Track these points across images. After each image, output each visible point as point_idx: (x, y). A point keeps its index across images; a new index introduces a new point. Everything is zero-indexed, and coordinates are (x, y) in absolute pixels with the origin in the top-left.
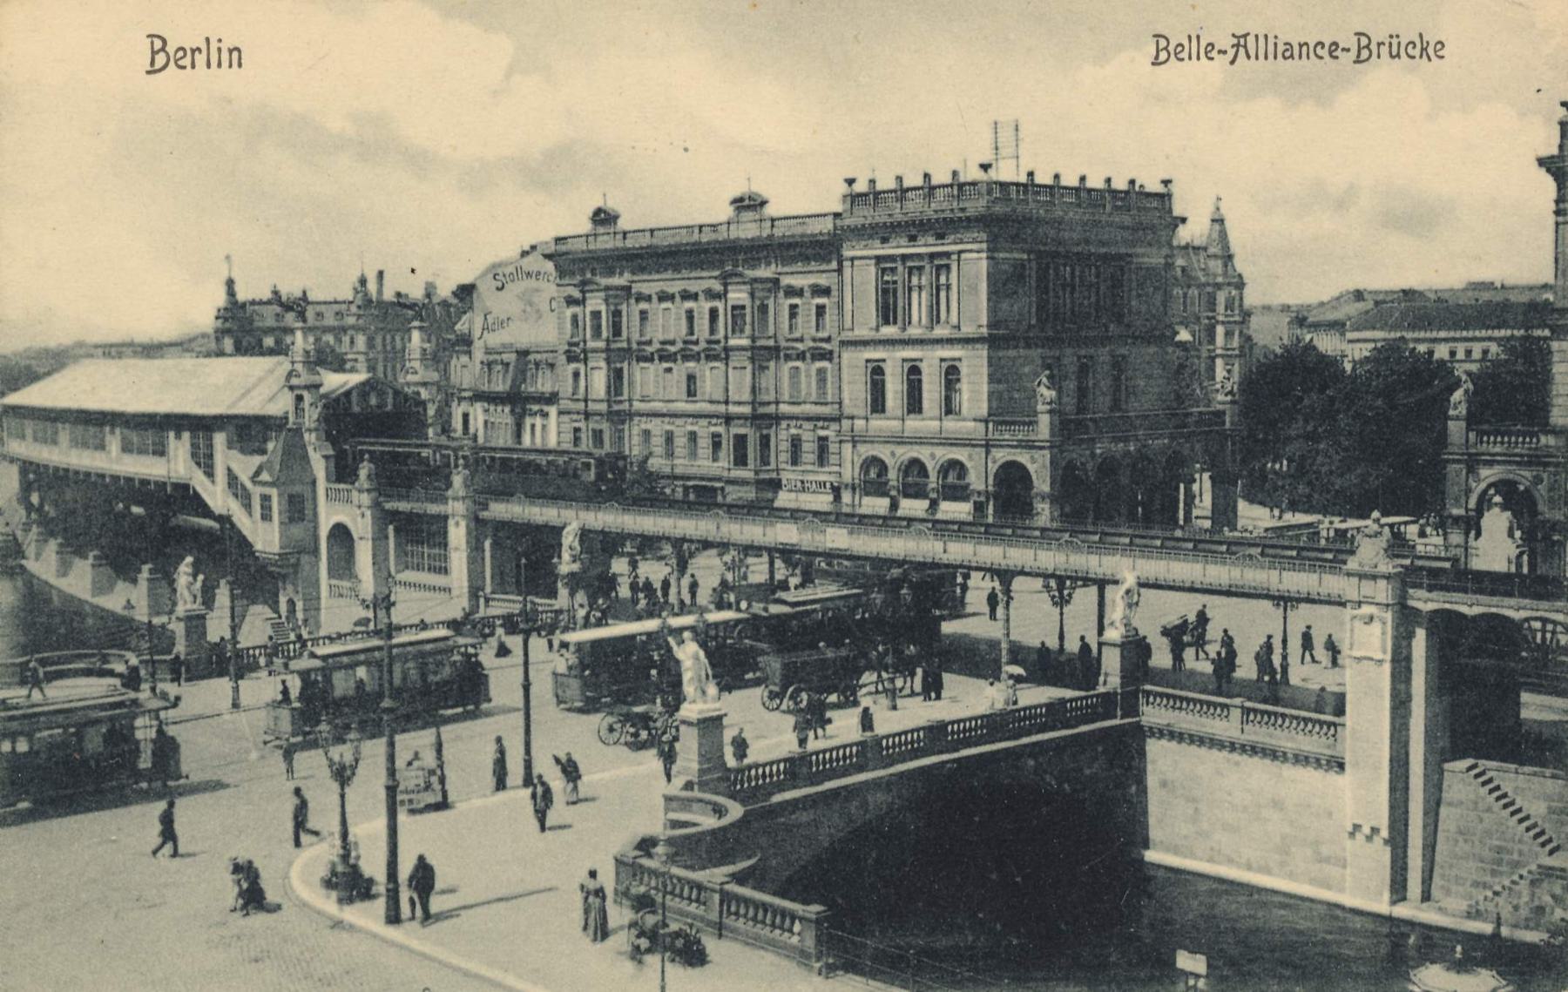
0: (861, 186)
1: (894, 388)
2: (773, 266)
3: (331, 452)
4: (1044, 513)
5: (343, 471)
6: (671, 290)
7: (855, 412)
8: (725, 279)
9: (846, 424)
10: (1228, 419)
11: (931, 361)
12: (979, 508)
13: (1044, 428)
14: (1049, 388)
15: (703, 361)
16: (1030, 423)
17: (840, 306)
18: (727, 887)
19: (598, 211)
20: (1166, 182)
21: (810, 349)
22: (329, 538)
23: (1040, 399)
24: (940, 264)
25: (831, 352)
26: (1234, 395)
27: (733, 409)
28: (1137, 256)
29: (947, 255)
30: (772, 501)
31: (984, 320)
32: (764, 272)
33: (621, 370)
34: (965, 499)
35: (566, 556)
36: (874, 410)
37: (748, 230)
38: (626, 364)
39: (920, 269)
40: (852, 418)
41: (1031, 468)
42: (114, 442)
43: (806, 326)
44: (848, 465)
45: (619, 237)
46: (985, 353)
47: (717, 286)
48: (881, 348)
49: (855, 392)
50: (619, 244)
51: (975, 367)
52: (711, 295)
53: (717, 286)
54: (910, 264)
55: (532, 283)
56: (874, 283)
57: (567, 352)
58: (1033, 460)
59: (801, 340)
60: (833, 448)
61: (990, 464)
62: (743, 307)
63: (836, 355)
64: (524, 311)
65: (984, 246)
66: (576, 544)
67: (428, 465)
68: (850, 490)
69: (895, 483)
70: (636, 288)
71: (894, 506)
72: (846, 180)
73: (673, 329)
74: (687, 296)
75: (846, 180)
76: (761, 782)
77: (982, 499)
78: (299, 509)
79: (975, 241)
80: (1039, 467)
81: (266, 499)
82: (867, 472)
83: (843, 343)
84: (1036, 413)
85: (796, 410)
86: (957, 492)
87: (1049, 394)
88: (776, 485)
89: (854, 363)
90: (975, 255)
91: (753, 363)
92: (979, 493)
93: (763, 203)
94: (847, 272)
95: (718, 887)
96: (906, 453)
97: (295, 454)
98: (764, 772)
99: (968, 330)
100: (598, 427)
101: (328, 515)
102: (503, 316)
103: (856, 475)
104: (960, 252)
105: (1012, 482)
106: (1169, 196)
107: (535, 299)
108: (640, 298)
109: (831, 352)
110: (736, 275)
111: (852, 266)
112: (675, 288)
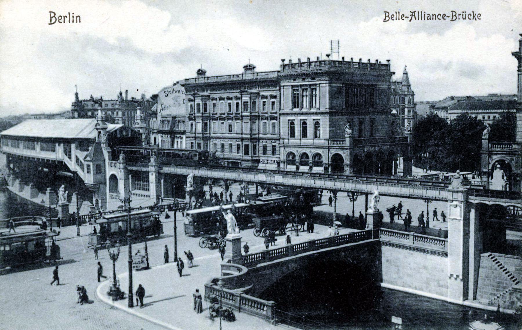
0: (287, 62)
1: (298, 129)
2: (257, 88)
4: (348, 171)
7: (285, 137)
8: (241, 93)
9: (282, 141)
10: (409, 140)
11: (310, 120)
12: (326, 169)
13: (348, 142)
14: (349, 129)
17: (280, 102)
19: (199, 70)
20: (388, 61)
21: (270, 116)
22: (109, 179)
24: (313, 88)
25: (277, 117)
26: (411, 131)
27: (244, 136)
29: (315, 85)
30: (257, 167)
32: (254, 91)
33: (207, 123)
34: (321, 166)
36: (291, 137)
37: (249, 76)
38: (208, 121)
39: (306, 89)
40: (284, 139)
41: (343, 156)
43: (268, 108)
44: (282, 155)
45: (206, 79)
46: (328, 117)
47: (239, 95)
48: (293, 116)
49: (285, 131)
50: (206, 81)
51: (325, 122)
52: (237, 98)
53: (239, 95)
54: (303, 88)
57: (189, 117)
58: (344, 153)
59: (267, 113)
60: (277, 149)
61: (329, 154)
62: (247, 102)
63: (278, 118)
65: (328, 82)
68: (283, 163)
70: (212, 96)
71: (298, 168)
74: (229, 98)
77: (327, 166)
78: (99, 169)
79: (324, 80)
80: (346, 155)
81: (88, 166)
82: (289, 157)
83: (281, 114)
84: (345, 137)
86: (319, 164)
87: (349, 131)
88: (258, 161)
89: (284, 121)
90: (324, 85)
91: (251, 121)
92: (326, 164)
94: (282, 90)
96: (302, 151)
99: (322, 110)
100: (199, 142)
101: (109, 172)
103: (285, 158)
104: (320, 84)
105: (337, 160)
106: (389, 65)
108: (213, 99)
109: (277, 117)
110: (245, 91)
111: (284, 88)
112: (225, 96)
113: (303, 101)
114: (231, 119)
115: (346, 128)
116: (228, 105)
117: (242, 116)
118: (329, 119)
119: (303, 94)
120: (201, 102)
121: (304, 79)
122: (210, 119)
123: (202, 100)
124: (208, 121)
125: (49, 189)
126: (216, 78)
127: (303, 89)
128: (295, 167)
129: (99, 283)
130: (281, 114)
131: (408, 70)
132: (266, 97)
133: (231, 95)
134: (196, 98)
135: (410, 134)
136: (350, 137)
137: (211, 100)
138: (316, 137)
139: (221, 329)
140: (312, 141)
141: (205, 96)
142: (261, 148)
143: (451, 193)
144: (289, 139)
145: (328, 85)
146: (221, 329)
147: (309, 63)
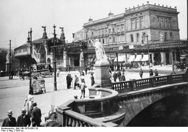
0: (128, 9)
2: (115, 22)
3: (48, 48)
5: (49, 51)
6: (100, 29)
7: (128, 42)
14: (162, 34)
15: (105, 38)
17: (125, 27)
18: (67, 112)
19: (90, 19)
20: (176, 7)
22: (47, 60)
23: (161, 36)
27: (110, 44)
28: (172, 18)
29: (143, 16)
32: (114, 23)
35: (81, 58)
40: (128, 43)
42: (22, 50)
45: (93, 22)
46: (150, 30)
47: (107, 27)
48: (132, 32)
50: (93, 23)
52: (106, 28)
53: (107, 27)
55: (82, 33)
56: (131, 24)
57: (86, 39)
63: (125, 34)
66: (83, 56)
76: (119, 89)
78: (43, 56)
79: (147, 13)
81: (38, 55)
83: (126, 32)
85: (119, 43)
89: (128, 35)
90: (147, 16)
94: (126, 22)
95: (62, 112)
97: (43, 49)
98: (118, 86)
99: (147, 27)
101: (47, 57)
102: (78, 38)
104: (144, 16)
106: (176, 9)
107: (83, 35)
108: (118, 26)
110: (109, 24)
111: (127, 21)
112: (100, 28)
113: (141, 25)
115: (160, 34)
116: (86, 34)
118: (151, 31)
119: (141, 20)
120: (111, 28)
121: (132, 16)
122: (116, 36)
123: (112, 27)
125: (79, 107)
126: (97, 21)
127: (141, 18)
129: (57, 108)
130: (126, 32)
132: (103, 29)
134: (109, 26)
137: (116, 26)
138: (138, 41)
140: (136, 43)
141: (113, 25)
143: (10, 44)
144: (136, 42)
147: (134, 8)
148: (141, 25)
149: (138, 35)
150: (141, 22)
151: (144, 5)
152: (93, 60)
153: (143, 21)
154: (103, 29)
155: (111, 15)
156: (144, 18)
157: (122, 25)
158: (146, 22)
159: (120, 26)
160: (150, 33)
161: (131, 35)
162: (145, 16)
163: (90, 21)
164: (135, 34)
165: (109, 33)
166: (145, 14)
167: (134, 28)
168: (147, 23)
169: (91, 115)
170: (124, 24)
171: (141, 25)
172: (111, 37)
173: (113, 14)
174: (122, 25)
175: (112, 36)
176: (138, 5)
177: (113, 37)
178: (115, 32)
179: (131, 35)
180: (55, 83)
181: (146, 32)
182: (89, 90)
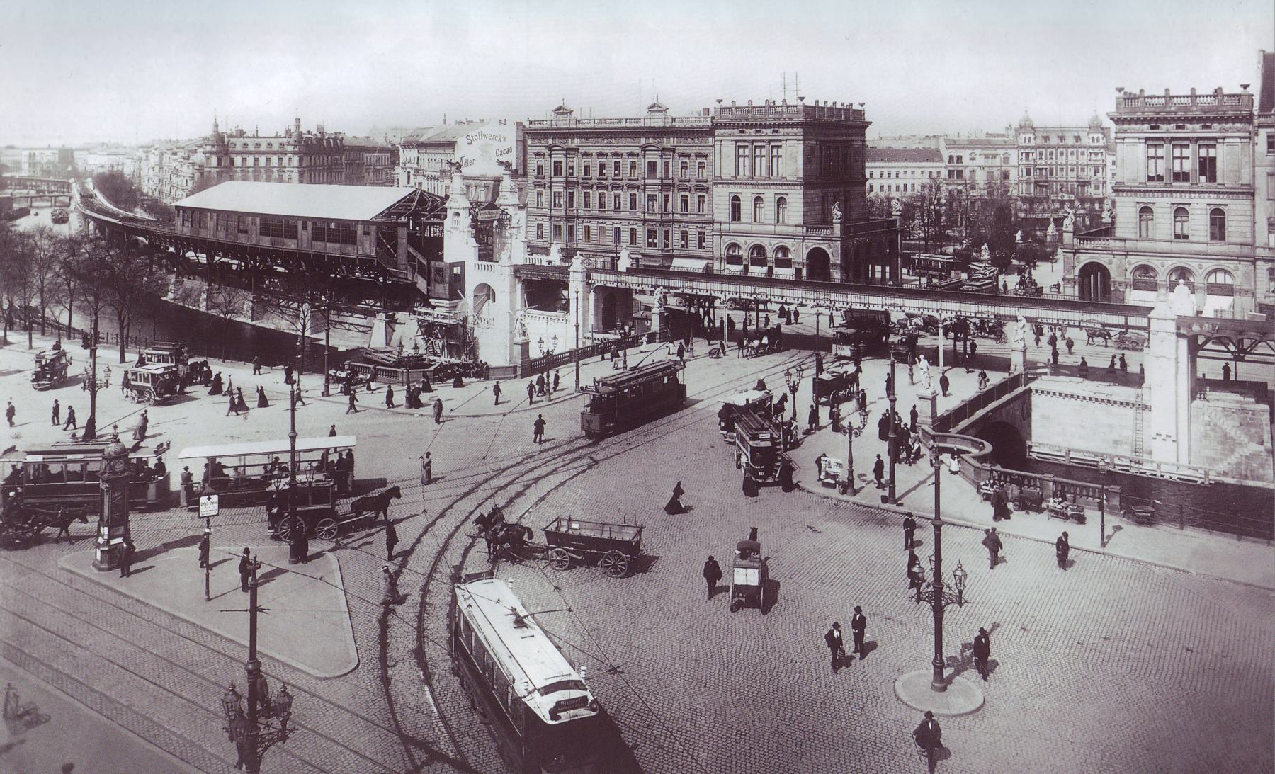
4: (836, 275)
7: (722, 220)
8: (551, 148)
9: (716, 226)
10: (898, 224)
12: (798, 271)
13: (837, 228)
16: (311, 181)
17: (713, 164)
20: (862, 105)
24: (775, 144)
25: (708, 188)
30: (669, 267)
31: (801, 174)
33: (573, 193)
34: (790, 267)
36: (734, 219)
37: (657, 122)
38: (575, 190)
39: (761, 147)
40: (721, 223)
41: (829, 252)
43: (692, 173)
44: (719, 246)
46: (802, 191)
49: (722, 211)
50: (573, 126)
51: (796, 199)
54: (772, 144)
58: (830, 247)
60: (708, 238)
61: (804, 249)
62: (561, 162)
64: (482, 155)
65: (801, 137)
67: (147, 195)
68: (719, 261)
69: (924, 280)
70: (582, 150)
71: (770, 270)
72: (1117, 89)
73: (982, 192)
74: (600, 155)
75: (1117, 89)
77: (801, 267)
79: (796, 135)
80: (834, 253)
82: (752, 253)
84: (831, 223)
86: (786, 263)
87: (839, 214)
88: (671, 257)
92: (799, 264)
93: (571, 112)
94: (717, 147)
96: (752, 241)
100: (557, 223)
103: (723, 253)
104: (786, 140)
105: (818, 260)
108: (586, 155)
109: (708, 188)
114: (687, 189)
117: (645, 185)
124: (670, 193)
128: (765, 269)
130: (714, 183)
131: (218, 122)
132: (688, 156)
133: (620, 150)
135: (900, 215)
136: (841, 223)
139: (6, 373)
142: (581, 231)
145: (802, 142)
146: (6, 373)
148: (770, 169)
149: (758, 200)
150: (772, 157)
151: (1169, 97)
152: (18, 222)
153: (778, 157)
154: (688, 156)
155: (563, 113)
156: (784, 146)
157: (699, 155)
158: (789, 163)
159: (625, 156)
160: (802, 201)
161: (731, 196)
162: (788, 142)
163: (561, 117)
164: (1205, 206)
165: (552, 175)
166: (788, 134)
167: (745, 173)
168: (791, 169)
169: (307, 505)
170: (622, 155)
171: (770, 169)
172: (657, 193)
173: (571, 112)
174: (699, 155)
175: (661, 191)
176: (1193, 89)
177: (664, 161)
178: (670, 177)
179: (734, 195)
180: (292, 434)
181: (1226, 205)
182: (997, 567)
